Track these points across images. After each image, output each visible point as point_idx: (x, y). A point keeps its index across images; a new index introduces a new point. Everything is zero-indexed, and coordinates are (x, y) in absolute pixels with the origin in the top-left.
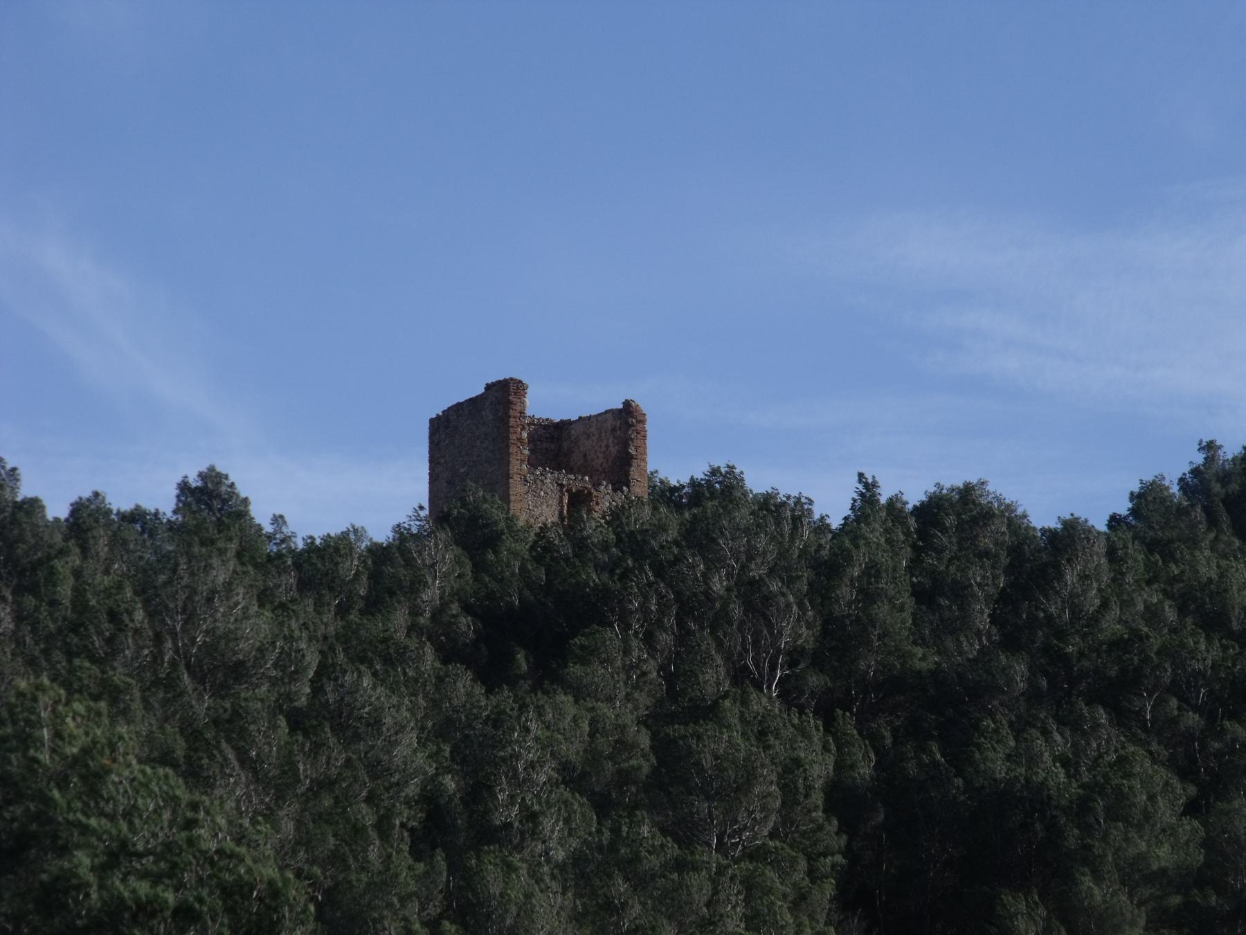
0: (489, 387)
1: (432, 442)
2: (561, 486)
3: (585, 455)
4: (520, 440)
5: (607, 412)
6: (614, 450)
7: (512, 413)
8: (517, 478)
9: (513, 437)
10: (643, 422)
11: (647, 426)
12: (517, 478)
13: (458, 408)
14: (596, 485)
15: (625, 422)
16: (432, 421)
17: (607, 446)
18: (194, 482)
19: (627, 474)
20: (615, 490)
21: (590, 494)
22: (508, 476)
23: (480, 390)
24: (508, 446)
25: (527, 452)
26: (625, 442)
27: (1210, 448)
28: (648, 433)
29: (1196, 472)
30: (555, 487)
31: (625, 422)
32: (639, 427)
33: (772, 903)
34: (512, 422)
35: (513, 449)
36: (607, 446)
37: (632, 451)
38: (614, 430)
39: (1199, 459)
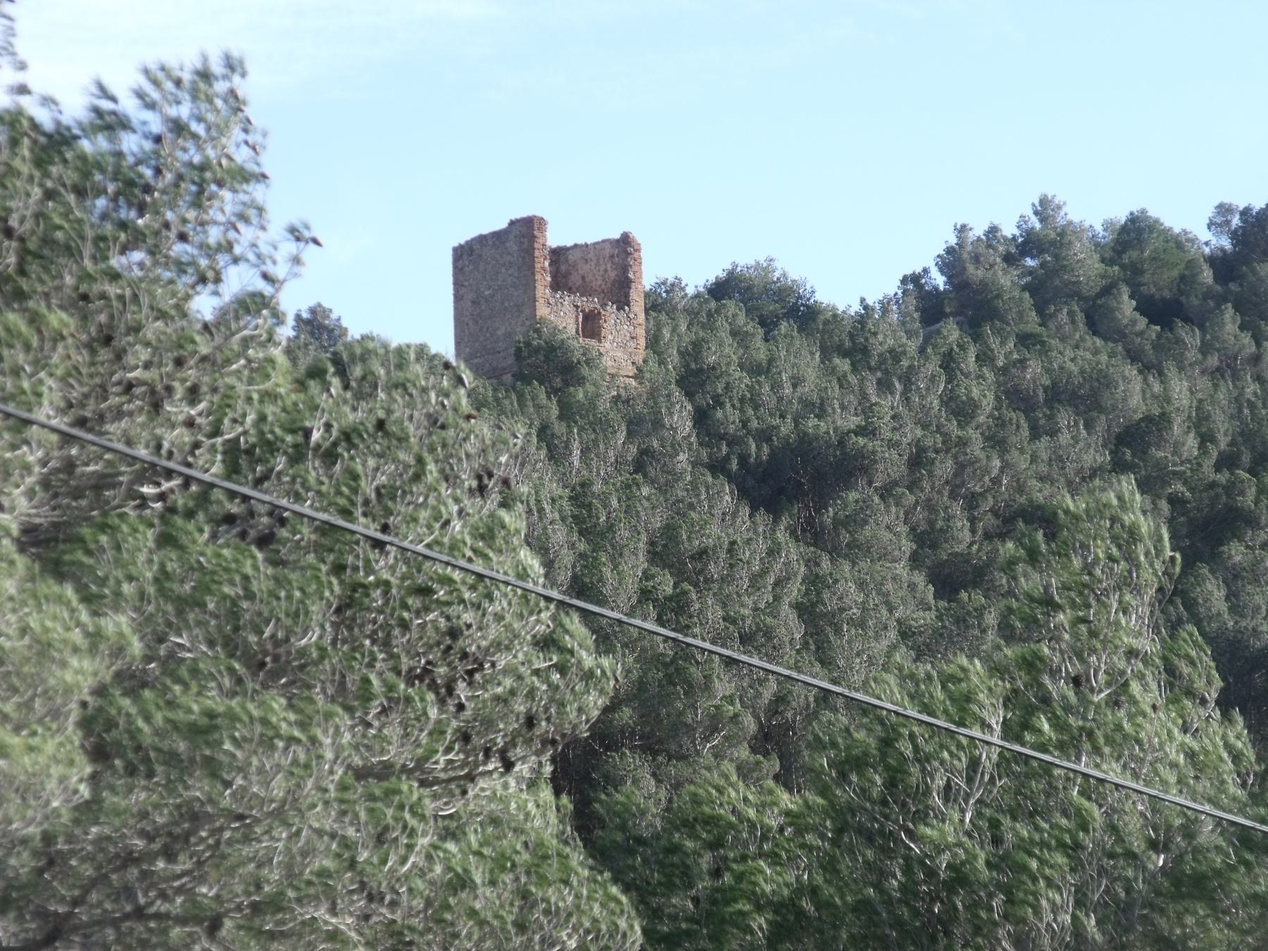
0: (512, 223)
1: (455, 267)
2: (577, 307)
3: (583, 278)
4: (543, 268)
5: (603, 241)
6: (612, 275)
7: (536, 245)
8: (542, 301)
9: (538, 266)
10: (638, 250)
11: (642, 254)
12: (542, 301)
13: (482, 239)
14: (604, 305)
15: (624, 247)
16: (455, 250)
17: (606, 271)
18: (305, 315)
19: (627, 296)
20: (618, 309)
21: (599, 313)
22: (534, 300)
23: (502, 224)
24: (533, 274)
25: (549, 279)
26: (625, 268)
27: (962, 230)
28: (643, 261)
29: (950, 250)
30: (573, 309)
31: (624, 247)
32: (636, 255)
33: (41, 382)
34: (537, 253)
35: (538, 277)
36: (606, 271)
37: (631, 276)
38: (612, 256)
39: (953, 241)
